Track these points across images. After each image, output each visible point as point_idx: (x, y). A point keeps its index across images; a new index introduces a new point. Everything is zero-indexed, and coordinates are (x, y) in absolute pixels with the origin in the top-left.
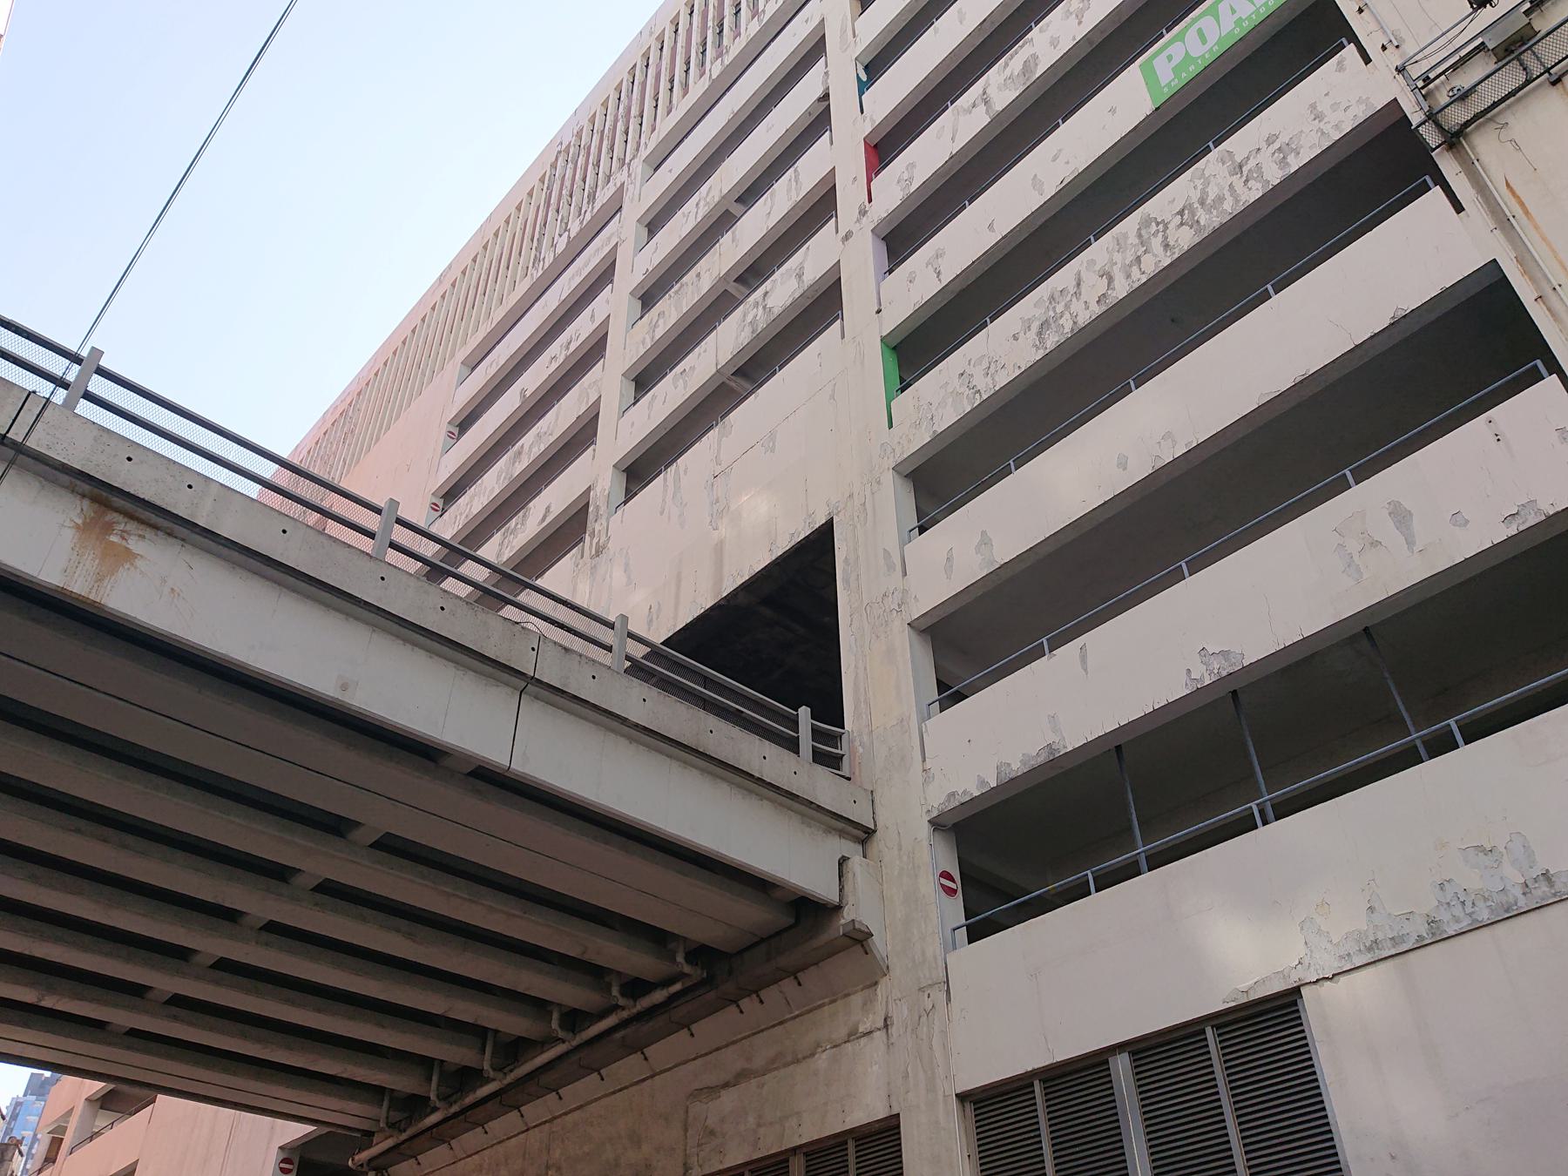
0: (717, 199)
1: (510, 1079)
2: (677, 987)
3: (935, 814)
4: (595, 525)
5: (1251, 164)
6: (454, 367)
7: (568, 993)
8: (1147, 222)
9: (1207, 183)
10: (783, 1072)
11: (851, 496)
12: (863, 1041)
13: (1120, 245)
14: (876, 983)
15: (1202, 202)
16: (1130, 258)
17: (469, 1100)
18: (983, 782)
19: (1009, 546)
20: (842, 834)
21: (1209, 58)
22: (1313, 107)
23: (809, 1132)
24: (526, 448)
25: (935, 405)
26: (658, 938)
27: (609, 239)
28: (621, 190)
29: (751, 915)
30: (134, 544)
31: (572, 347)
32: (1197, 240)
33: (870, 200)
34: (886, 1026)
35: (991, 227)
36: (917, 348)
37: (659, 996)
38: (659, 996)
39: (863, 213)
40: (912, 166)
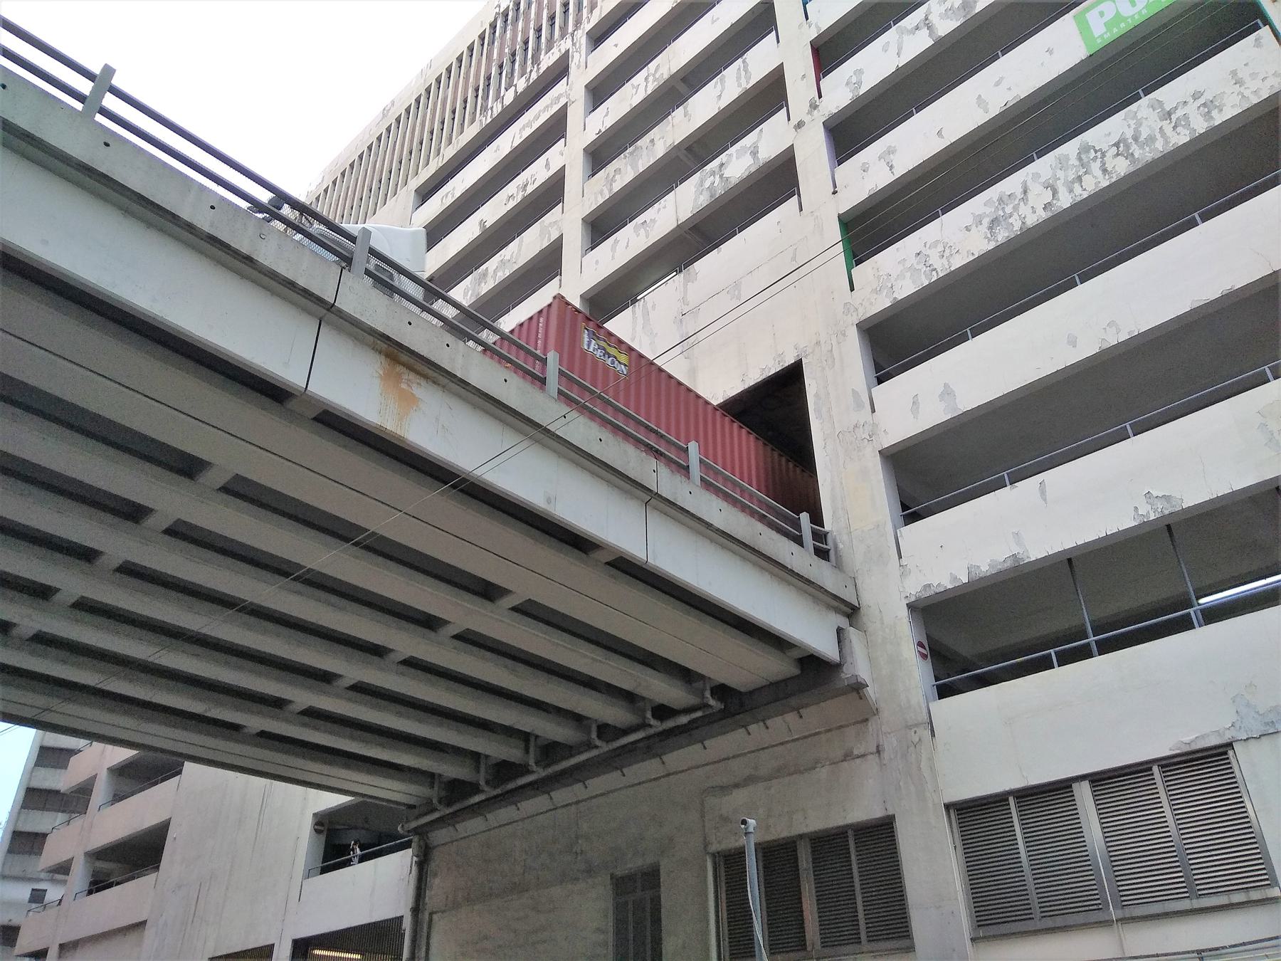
0: (666, 76)
1: (550, 770)
2: (699, 714)
3: (913, 599)
5: (1179, 113)
6: (407, 194)
7: (614, 714)
8: (1085, 148)
9: (1139, 124)
10: (787, 779)
11: (818, 343)
12: (858, 761)
13: (1063, 163)
14: (867, 720)
15: (1136, 139)
16: (1071, 176)
17: (511, 786)
18: (955, 578)
19: (972, 397)
20: (837, 610)
21: (1138, 19)
22: (1234, 73)
23: (816, 822)
24: (491, 271)
25: (894, 276)
26: (685, 675)
27: (558, 98)
28: (565, 58)
29: (771, 666)
31: (530, 189)
32: (1132, 169)
33: (820, 96)
34: (878, 752)
35: (939, 133)
36: (868, 230)
37: (684, 720)
38: (684, 720)
39: (814, 106)
40: (859, 72)
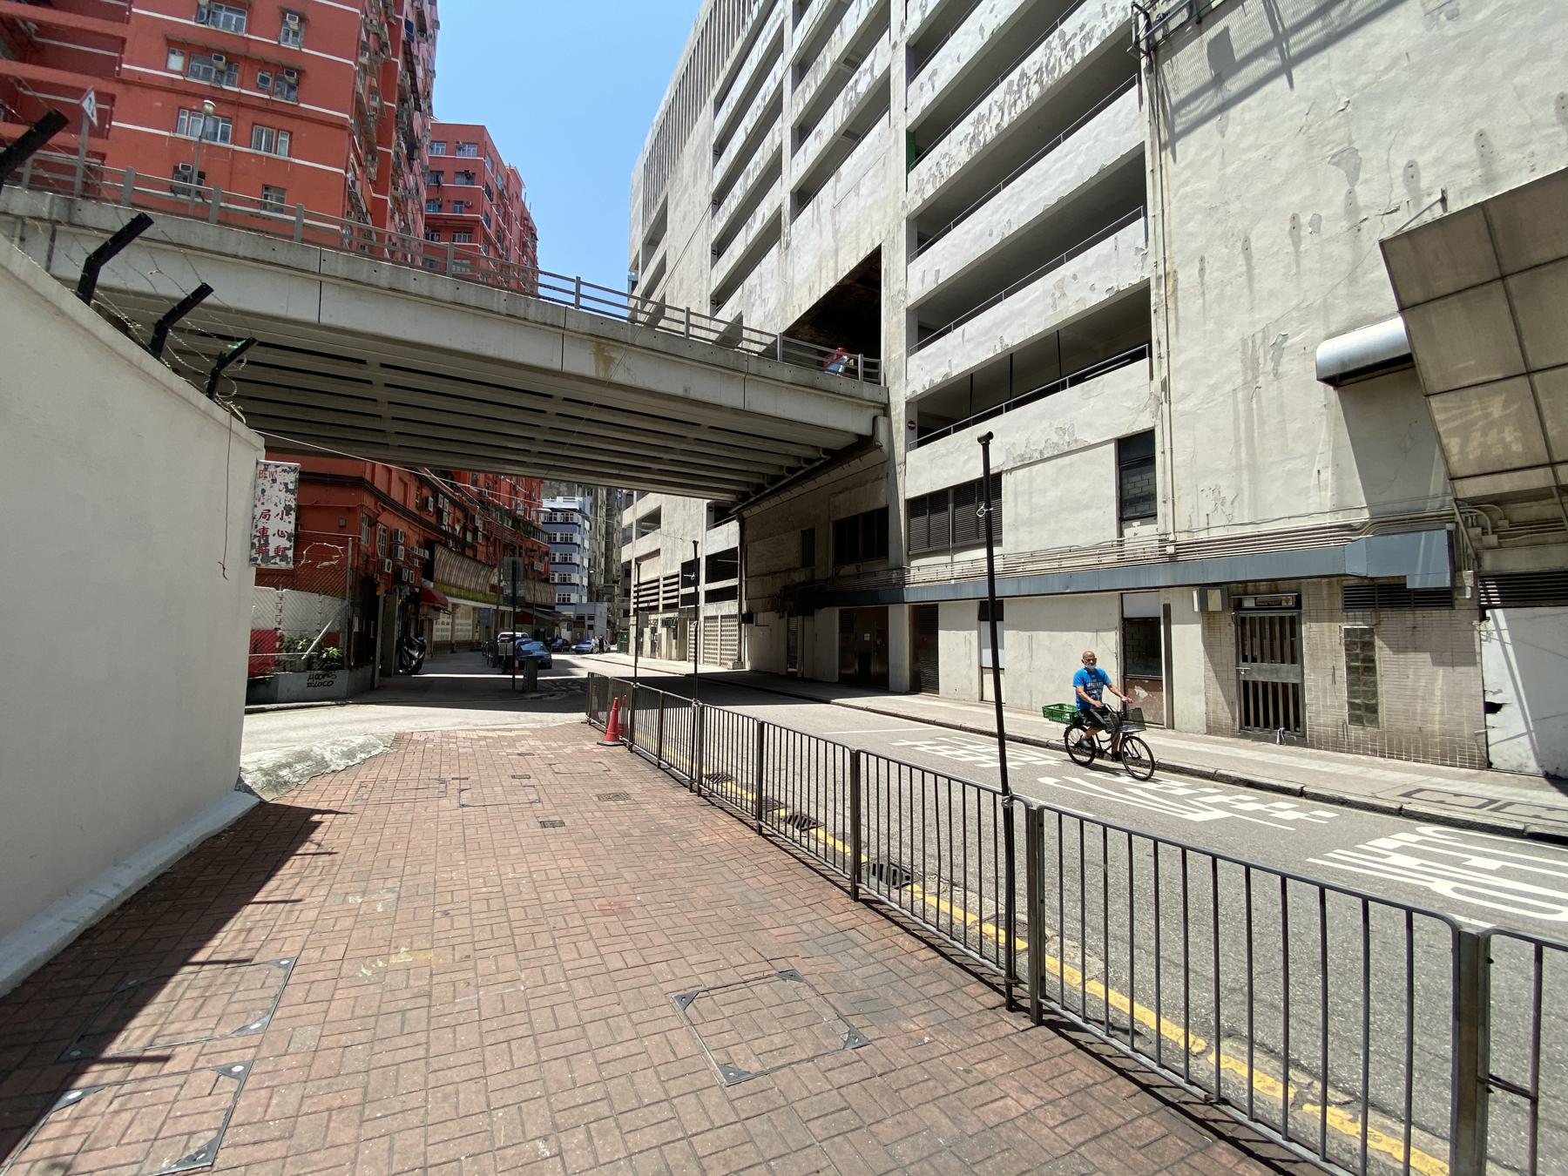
4: (785, 229)
23: (864, 509)
30: (613, 355)
